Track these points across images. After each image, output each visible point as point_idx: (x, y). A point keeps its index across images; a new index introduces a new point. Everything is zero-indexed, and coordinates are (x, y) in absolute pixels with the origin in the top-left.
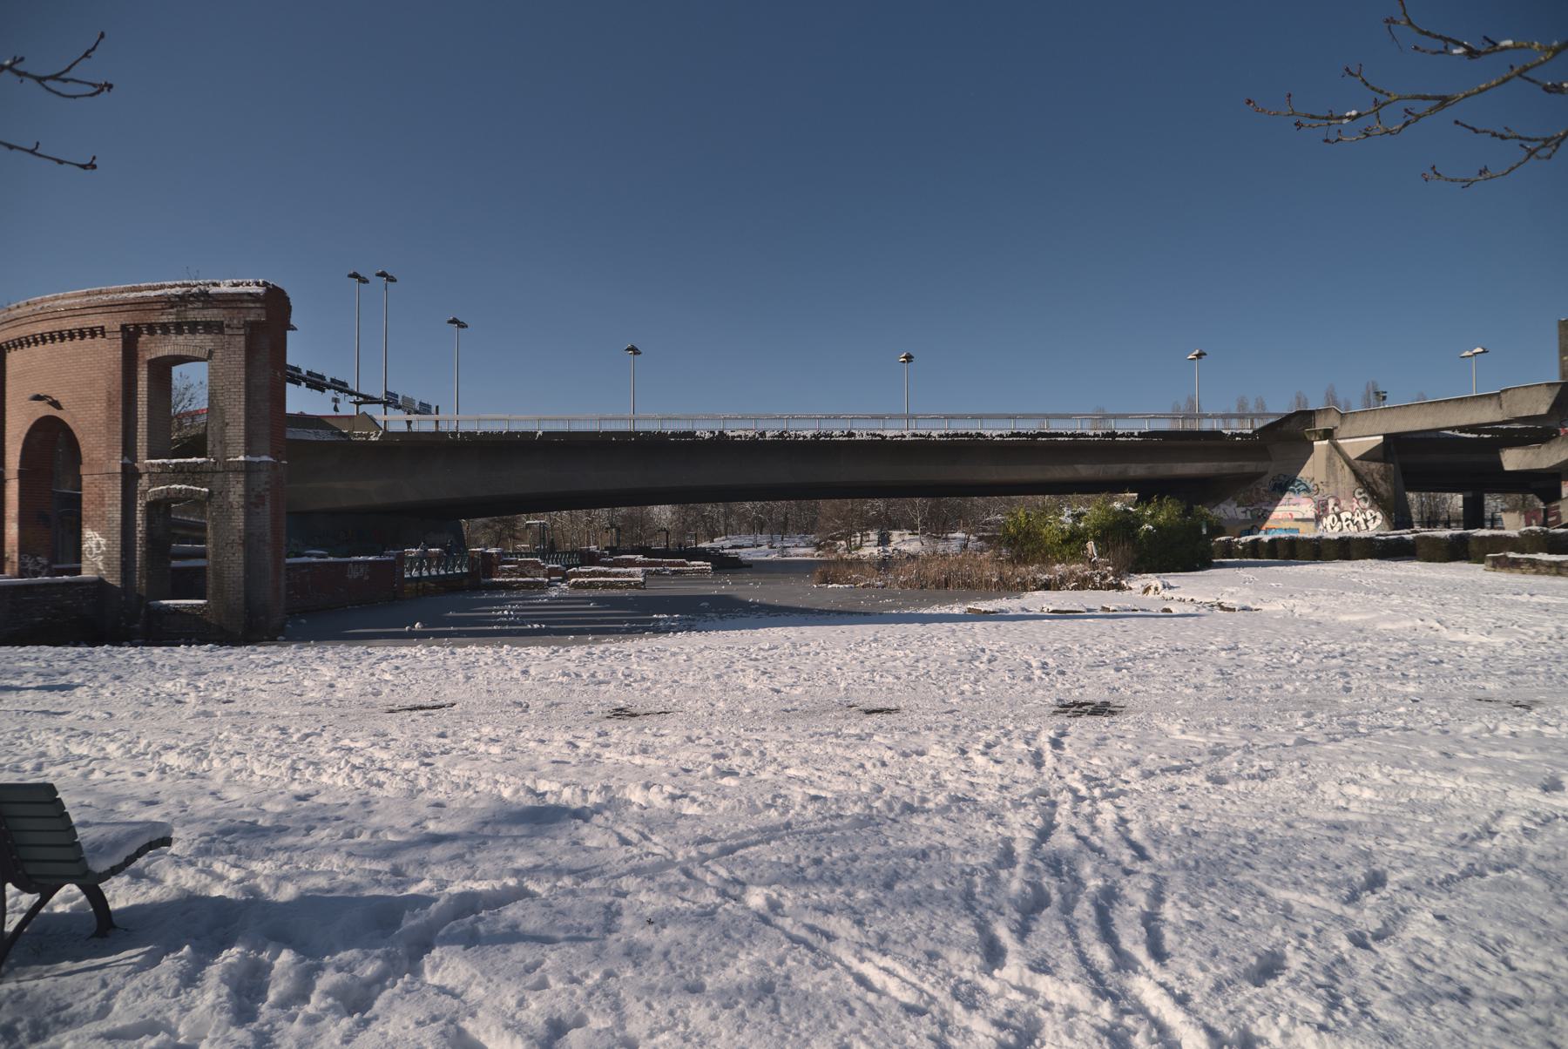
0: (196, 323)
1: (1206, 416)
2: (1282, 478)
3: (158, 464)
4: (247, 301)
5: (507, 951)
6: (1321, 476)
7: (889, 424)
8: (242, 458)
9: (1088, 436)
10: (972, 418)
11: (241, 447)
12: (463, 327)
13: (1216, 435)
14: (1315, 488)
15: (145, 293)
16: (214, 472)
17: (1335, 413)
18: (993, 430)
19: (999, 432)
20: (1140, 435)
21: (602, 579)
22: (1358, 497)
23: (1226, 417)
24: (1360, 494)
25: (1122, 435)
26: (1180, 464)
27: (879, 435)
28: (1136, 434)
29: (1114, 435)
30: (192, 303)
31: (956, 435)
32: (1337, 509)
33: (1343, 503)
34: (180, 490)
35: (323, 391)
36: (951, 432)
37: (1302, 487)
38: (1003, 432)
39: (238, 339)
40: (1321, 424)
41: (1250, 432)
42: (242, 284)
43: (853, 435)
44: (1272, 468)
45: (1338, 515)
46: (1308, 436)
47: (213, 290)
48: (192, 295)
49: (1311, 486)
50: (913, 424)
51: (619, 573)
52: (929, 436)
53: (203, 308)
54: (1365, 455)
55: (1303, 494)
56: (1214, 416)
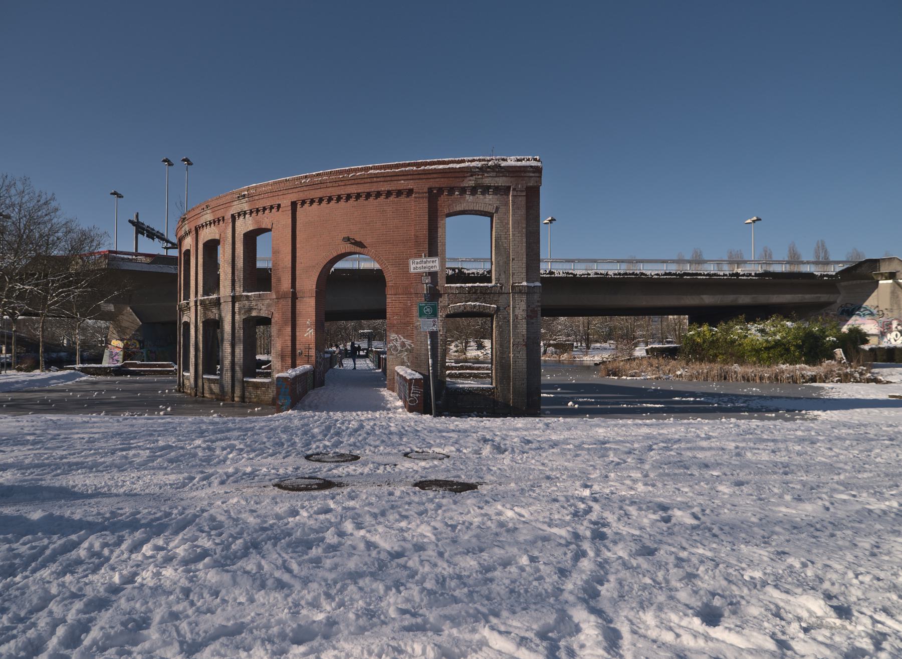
0: (489, 187)
1: (803, 263)
2: (849, 305)
3: (457, 287)
4: (529, 172)
5: (657, 637)
6: (885, 304)
7: (578, 266)
8: (525, 284)
9: (719, 276)
10: (618, 262)
11: (524, 275)
12: (120, 197)
13: (810, 275)
15: (451, 166)
16: (500, 293)
17: (897, 261)
18: (652, 270)
19: (657, 272)
20: (756, 275)
21: (468, 371)
23: (719, 263)
25: (743, 275)
26: (775, 296)
27: (571, 274)
28: (753, 274)
29: (737, 275)
30: (488, 172)
31: (626, 274)
34: (475, 306)
35: (153, 239)
36: (622, 272)
37: (868, 312)
38: (660, 272)
39: (520, 199)
40: (885, 269)
41: (834, 273)
42: (524, 159)
43: (553, 273)
44: (840, 300)
46: (875, 277)
47: (503, 164)
48: (489, 167)
49: (875, 312)
50: (595, 266)
51: (480, 367)
52: (607, 274)
53: (496, 177)
55: (868, 317)
56: (808, 263)
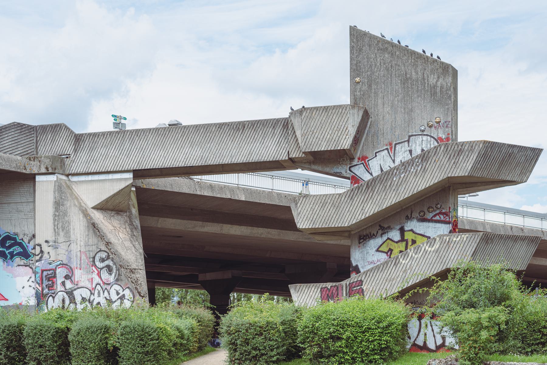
14: (38, 249)
22: (99, 265)
24: (102, 260)
32: (69, 285)
33: (78, 275)
45: (70, 293)
54: (107, 201)
55: (18, 260)
